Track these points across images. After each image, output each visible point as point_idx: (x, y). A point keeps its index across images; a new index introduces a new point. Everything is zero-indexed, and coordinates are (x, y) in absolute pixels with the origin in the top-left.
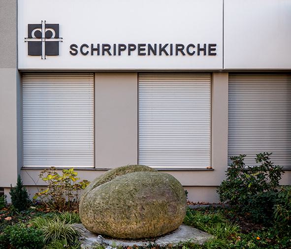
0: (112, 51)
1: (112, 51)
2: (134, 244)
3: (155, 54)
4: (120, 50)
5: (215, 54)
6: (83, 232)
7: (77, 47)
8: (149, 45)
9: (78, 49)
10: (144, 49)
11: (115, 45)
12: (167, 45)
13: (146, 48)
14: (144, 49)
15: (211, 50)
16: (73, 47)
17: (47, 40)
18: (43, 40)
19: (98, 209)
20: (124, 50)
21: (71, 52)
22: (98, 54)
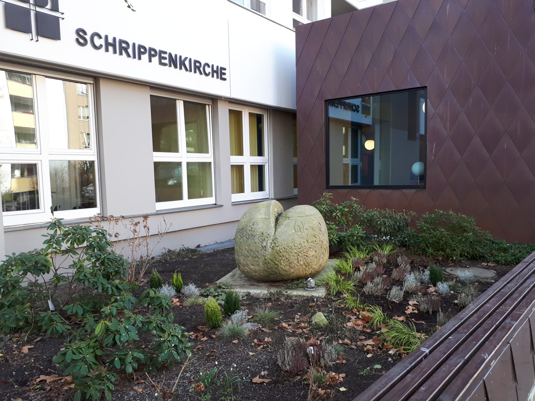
0: (130, 51)
1: (130, 51)
2: (245, 291)
3: (176, 67)
4: (140, 53)
5: (225, 79)
6: (36, 388)
7: (85, 33)
8: (170, 55)
9: (88, 37)
10: (165, 58)
11: (134, 44)
12: (186, 58)
13: (167, 56)
14: (165, 58)
15: (220, 73)
16: (81, 33)
17: (38, 9)
18: (32, 7)
19: (301, 249)
20: (144, 53)
21: (77, 40)
22: (115, 52)
